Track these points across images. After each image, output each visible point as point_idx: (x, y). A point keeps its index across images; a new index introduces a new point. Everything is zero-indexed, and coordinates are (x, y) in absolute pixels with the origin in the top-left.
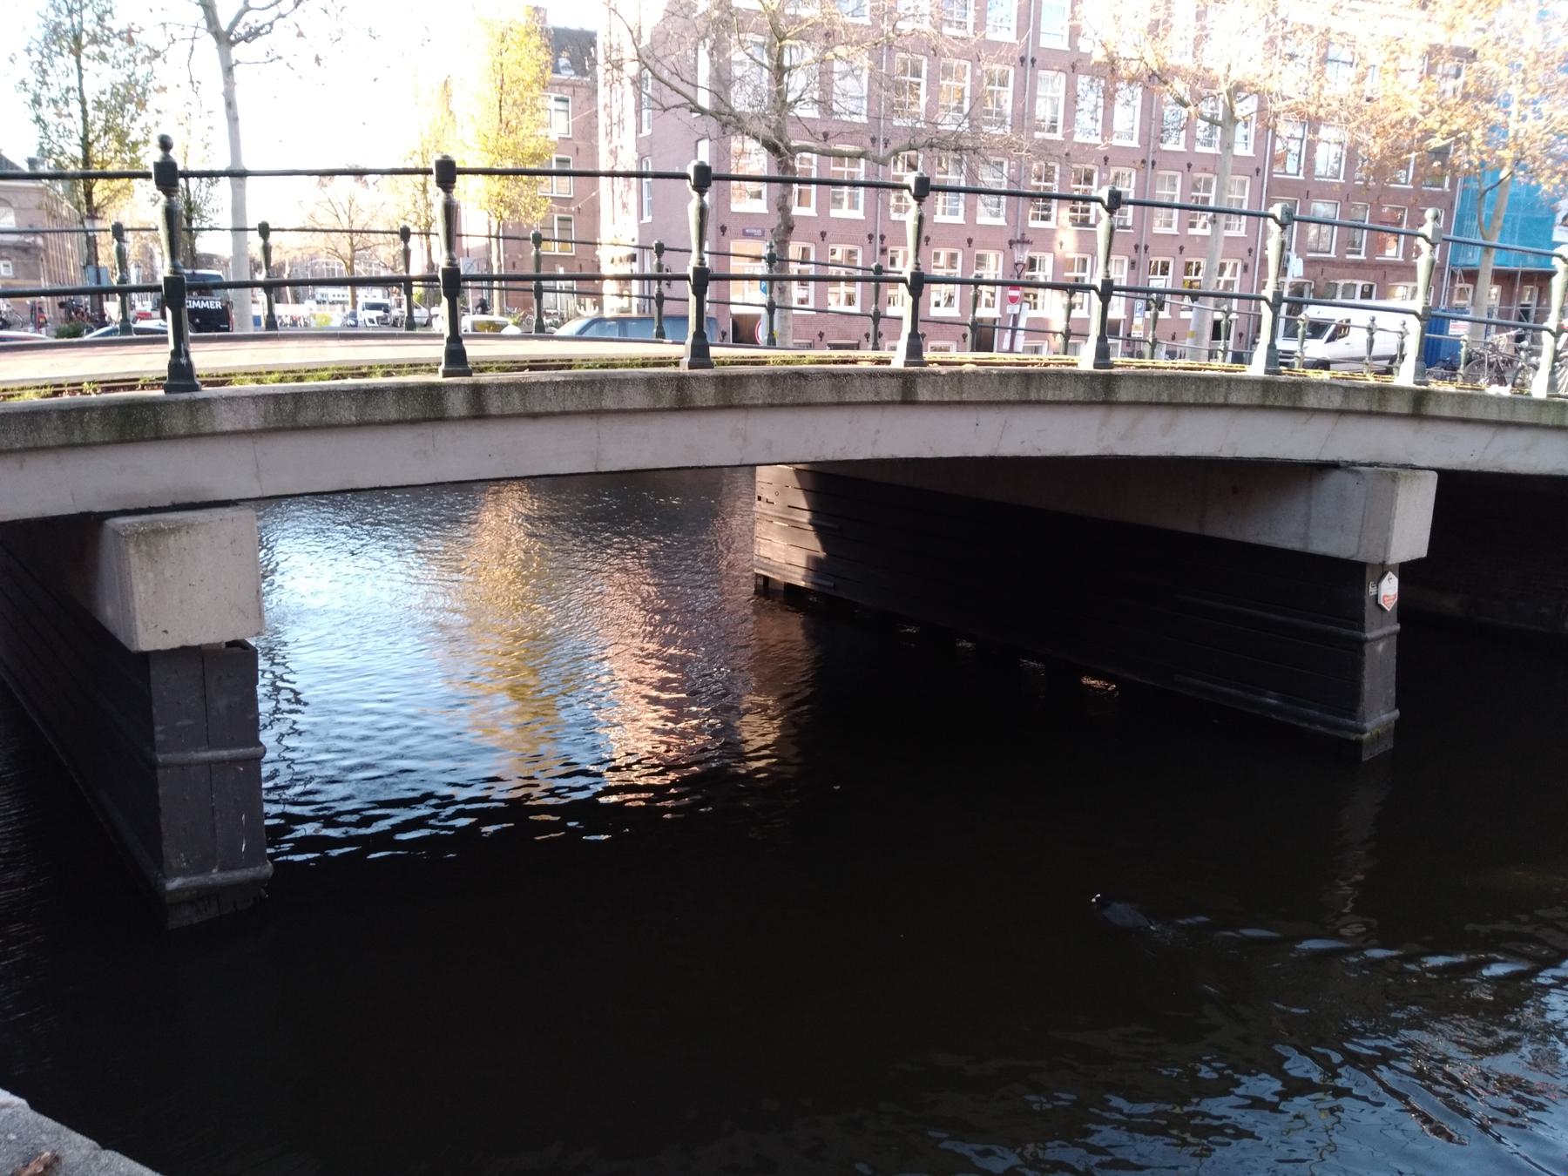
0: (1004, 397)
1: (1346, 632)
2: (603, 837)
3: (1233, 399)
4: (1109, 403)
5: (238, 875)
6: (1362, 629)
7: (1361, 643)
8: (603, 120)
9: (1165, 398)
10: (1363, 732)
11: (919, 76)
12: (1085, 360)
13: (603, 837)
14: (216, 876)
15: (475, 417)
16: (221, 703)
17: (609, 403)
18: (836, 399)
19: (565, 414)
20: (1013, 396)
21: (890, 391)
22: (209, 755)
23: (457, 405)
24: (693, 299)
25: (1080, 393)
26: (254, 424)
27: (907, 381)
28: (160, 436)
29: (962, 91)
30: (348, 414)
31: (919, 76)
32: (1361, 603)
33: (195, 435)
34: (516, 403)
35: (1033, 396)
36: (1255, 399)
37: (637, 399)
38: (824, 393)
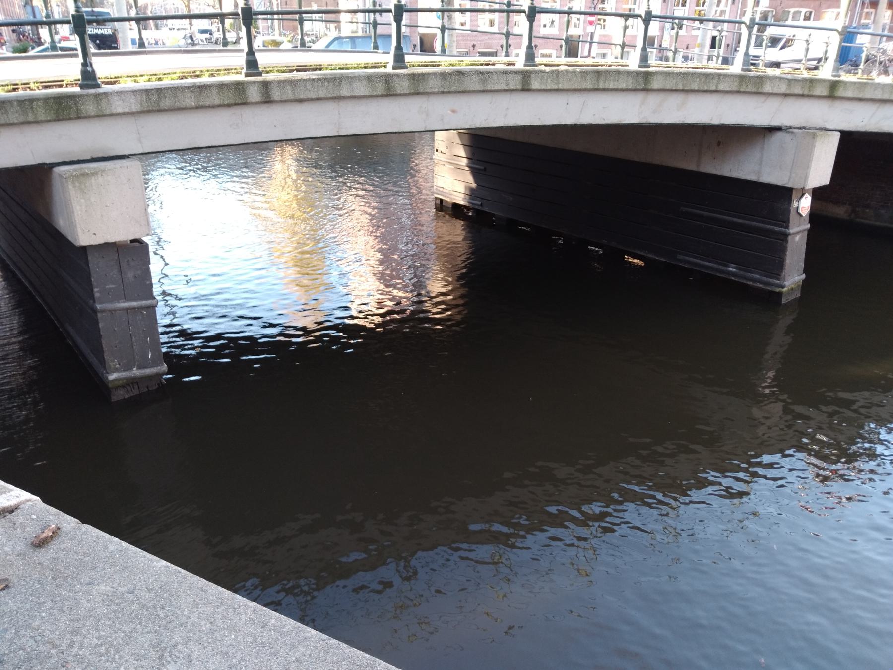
0: (584, 87)
1: (777, 229)
5: (148, 371)
7: (786, 235)
9: (680, 87)
10: (783, 287)
14: (136, 372)
17: (345, 92)
19: (319, 99)
33: (100, 116)
34: (289, 94)
35: (601, 86)
37: (361, 89)
38: (473, 84)
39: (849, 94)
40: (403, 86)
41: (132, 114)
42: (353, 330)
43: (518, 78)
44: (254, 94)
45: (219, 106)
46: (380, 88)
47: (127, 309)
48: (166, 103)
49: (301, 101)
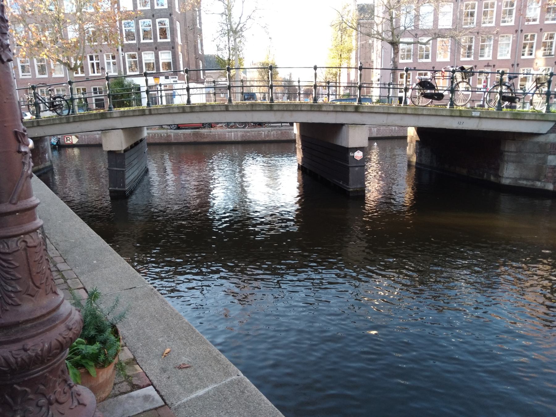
0: (247, 109)
1: (344, 163)
2: (547, 251)
3: (303, 109)
4: (271, 110)
5: (120, 189)
6: (348, 164)
7: (348, 168)
8: (445, 39)
9: (285, 109)
10: (349, 189)
11: (107, 63)
12: (268, 102)
13: (547, 251)
14: (117, 188)
15: (142, 115)
16: (118, 161)
17: (171, 111)
18: (404, 112)
19: (164, 114)
20: (249, 109)
21: (223, 108)
22: (115, 169)
23: (147, 112)
24: (314, 90)
25: (265, 108)
26: (118, 116)
27: (271, 106)
28: (107, 118)
29: (23, 72)
30: (131, 114)
31: (107, 63)
32: (348, 157)
33: (111, 118)
34: (156, 112)
35: (254, 109)
36: (309, 109)
37: (176, 111)
38: (210, 109)
39: (366, 110)
40: (188, 110)
41: (224, 111)
42: (198, 264)
43: (224, 107)
44: (147, 112)
45: (333, 111)
46: (181, 110)
47: (116, 170)
48: (126, 114)
49: (161, 114)
